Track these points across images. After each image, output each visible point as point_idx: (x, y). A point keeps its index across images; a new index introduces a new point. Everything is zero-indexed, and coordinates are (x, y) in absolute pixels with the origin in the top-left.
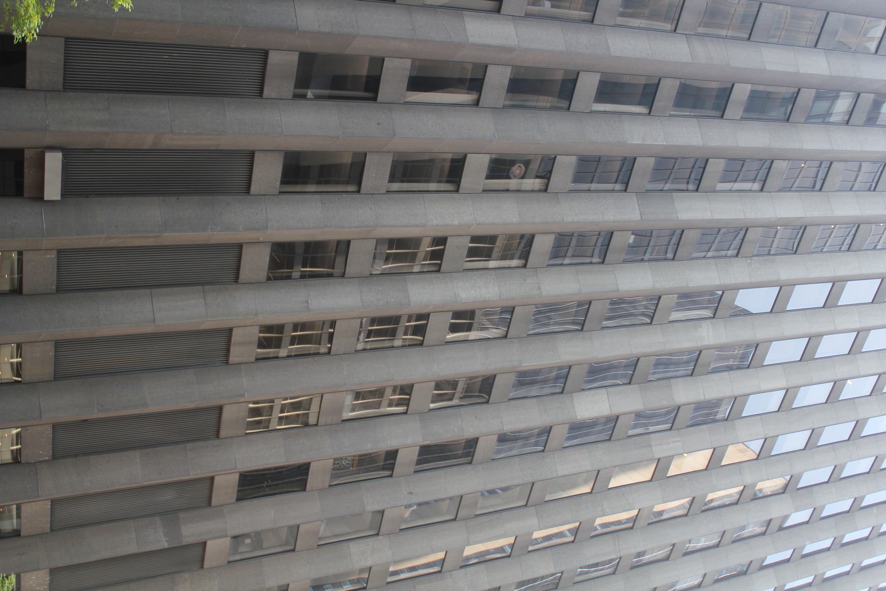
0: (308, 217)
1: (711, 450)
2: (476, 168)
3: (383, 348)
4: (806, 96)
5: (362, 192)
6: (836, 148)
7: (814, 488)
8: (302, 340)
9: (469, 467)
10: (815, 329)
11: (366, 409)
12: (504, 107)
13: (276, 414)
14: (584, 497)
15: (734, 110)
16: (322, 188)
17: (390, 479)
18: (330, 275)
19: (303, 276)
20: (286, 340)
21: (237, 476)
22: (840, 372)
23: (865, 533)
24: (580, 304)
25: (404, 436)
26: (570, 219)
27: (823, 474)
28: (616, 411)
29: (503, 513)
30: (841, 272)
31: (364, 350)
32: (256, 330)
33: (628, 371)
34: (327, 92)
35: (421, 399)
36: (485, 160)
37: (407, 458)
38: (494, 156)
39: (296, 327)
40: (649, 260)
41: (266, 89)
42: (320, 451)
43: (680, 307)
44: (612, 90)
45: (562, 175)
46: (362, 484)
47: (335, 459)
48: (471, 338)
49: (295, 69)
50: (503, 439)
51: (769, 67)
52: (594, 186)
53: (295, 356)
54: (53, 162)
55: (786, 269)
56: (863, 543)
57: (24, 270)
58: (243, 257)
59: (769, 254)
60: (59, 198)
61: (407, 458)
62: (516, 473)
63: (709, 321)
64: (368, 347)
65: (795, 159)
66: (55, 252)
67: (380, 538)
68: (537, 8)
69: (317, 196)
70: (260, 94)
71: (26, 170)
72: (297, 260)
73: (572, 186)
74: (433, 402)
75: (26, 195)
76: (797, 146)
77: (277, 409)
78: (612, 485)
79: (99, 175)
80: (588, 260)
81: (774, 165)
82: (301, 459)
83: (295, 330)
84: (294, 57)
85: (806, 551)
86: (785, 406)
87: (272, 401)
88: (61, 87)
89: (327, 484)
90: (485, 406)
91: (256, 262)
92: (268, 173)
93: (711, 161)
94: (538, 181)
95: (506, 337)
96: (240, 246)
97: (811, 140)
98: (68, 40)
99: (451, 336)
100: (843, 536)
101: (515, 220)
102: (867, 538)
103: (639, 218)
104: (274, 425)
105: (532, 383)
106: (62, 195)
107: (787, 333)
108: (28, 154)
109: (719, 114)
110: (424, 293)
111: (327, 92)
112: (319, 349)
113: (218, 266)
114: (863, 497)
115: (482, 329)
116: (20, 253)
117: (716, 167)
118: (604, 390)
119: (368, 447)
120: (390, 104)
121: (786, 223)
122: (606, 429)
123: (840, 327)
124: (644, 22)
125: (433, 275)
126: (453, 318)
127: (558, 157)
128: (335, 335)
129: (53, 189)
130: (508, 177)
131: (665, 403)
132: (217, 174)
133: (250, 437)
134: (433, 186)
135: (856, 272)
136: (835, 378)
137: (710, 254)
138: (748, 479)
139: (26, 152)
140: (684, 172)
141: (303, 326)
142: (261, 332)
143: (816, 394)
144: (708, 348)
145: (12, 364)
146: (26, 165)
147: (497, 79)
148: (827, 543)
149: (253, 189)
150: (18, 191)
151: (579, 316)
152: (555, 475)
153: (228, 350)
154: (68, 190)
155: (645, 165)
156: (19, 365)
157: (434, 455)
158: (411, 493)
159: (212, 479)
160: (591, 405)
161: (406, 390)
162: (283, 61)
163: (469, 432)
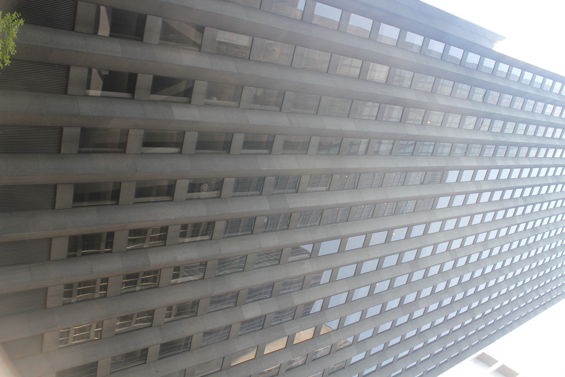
0: (90, 220)
1: (314, 328)
2: (182, 186)
3: (130, 292)
5: (120, 204)
7: (366, 341)
8: (84, 291)
10: (360, 259)
15: (313, 149)
19: (83, 254)
20: (75, 292)
23: (391, 360)
25: (152, 340)
27: (369, 333)
28: (264, 313)
30: (370, 229)
31: (141, 290)
35: (160, 318)
36: (187, 182)
39: (80, 284)
40: (279, 230)
43: (293, 254)
45: (228, 189)
47: (112, 358)
48: (179, 282)
50: (206, 334)
52: (250, 193)
53: (81, 301)
55: (344, 230)
61: (154, 351)
64: (143, 288)
68: (218, 101)
69: (94, 208)
70: (59, 151)
73: (234, 194)
74: (166, 318)
78: (232, 365)
83: (80, 286)
91: (60, 248)
96: (50, 240)
99: (173, 281)
110: (158, 258)
114: (389, 342)
115: (184, 276)
119: (131, 348)
121: (340, 206)
125: (162, 248)
126: (174, 271)
127: (225, 179)
128: (108, 286)
130: (199, 191)
137: (308, 225)
138: (334, 340)
141: (148, 273)
142: (65, 288)
144: (309, 274)
147: (191, 138)
148: (374, 368)
149: (57, 206)
158: (157, 371)
160: (252, 311)
161: (151, 313)
163: (187, 333)
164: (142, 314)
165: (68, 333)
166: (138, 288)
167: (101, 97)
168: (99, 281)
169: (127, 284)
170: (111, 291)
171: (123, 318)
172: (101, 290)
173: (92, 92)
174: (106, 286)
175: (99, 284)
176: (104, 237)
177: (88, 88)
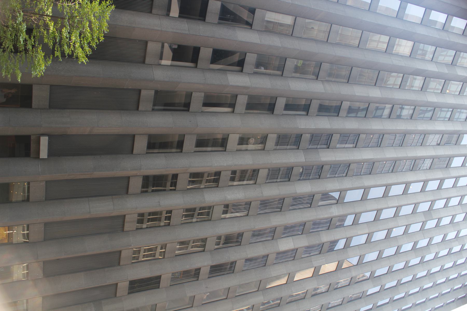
0: (159, 164)
1: (337, 262)
4: (373, 106)
6: (386, 128)
8: (153, 220)
9: (232, 274)
10: (379, 207)
11: (147, 257)
12: (245, 113)
13: (142, 253)
14: (283, 286)
15: (343, 113)
16: (161, 151)
17: (197, 281)
18: (165, 190)
19: (153, 191)
20: (145, 220)
21: (128, 282)
22: (390, 225)
23: (403, 295)
24: (309, 196)
26: (275, 162)
27: (384, 270)
28: (296, 247)
29: (248, 295)
30: (390, 182)
32: (136, 215)
33: (301, 229)
34: (162, 108)
35: (210, 245)
36: (237, 137)
37: (205, 271)
38: (241, 135)
39: (150, 214)
40: (312, 179)
41: (140, 106)
42: (166, 269)
43: (322, 199)
44: (291, 106)
45: (271, 143)
46: (185, 284)
47: (173, 273)
48: (227, 217)
49: (153, 98)
50: (247, 260)
51: (357, 94)
53: (150, 227)
54: (44, 141)
55: (367, 181)
56: (402, 299)
57: (31, 191)
58: (130, 182)
59: (360, 175)
60: (47, 157)
61: (205, 271)
62: (253, 277)
63: (335, 205)
64: (199, 220)
65: (368, 133)
66: (44, 182)
67: (193, 308)
69: (163, 154)
71: (32, 145)
72: (156, 183)
75: (31, 156)
76: (370, 128)
77: (142, 251)
79: (65, 147)
80: (275, 180)
81: (360, 136)
82: (157, 274)
83: (149, 216)
84: (153, 92)
85: (379, 304)
86: (368, 241)
87: (140, 248)
88: (48, 107)
89: (169, 285)
90: (239, 247)
91: (136, 185)
92: (141, 144)
93: (334, 135)
94: (260, 145)
95: (247, 215)
96: (129, 178)
97: (376, 125)
98: (51, 86)
100: (394, 297)
101: (251, 163)
102: (403, 297)
103: (304, 160)
104: (157, 256)
105: (258, 235)
106: (48, 156)
107: (368, 209)
108: (32, 138)
109: (337, 114)
110: (212, 197)
111: (162, 108)
112: (142, 226)
113: (118, 187)
114: (402, 279)
115: (232, 213)
116: (29, 184)
117: (336, 137)
118: (291, 238)
120: (195, 113)
121: (365, 161)
122: (291, 255)
123: (390, 206)
124: (272, 71)
125: (215, 189)
129: (44, 154)
130: (247, 144)
131: (318, 242)
132: (120, 145)
133: (134, 264)
134: (209, 149)
135: (396, 181)
136: (389, 228)
137: (336, 176)
139: (32, 136)
140: (324, 140)
143: (380, 235)
145: (24, 234)
146: (32, 142)
147: (242, 101)
148: (387, 300)
149: (135, 152)
150: (27, 154)
151: (279, 205)
152: (271, 276)
153: (124, 225)
154: (51, 153)
155: (306, 137)
156: (28, 234)
157: (217, 270)
159: (117, 284)
160: (286, 244)
161: (204, 240)
162: (147, 94)
163: (232, 259)
164: (198, 240)
165: (139, 252)
166: (194, 220)
167: (171, 66)
168: (164, 213)
169: (186, 216)
170: (174, 221)
171: (182, 243)
172: (165, 220)
173: (164, 62)
174: (170, 217)
175: (164, 215)
176: (170, 178)
177: (161, 58)
